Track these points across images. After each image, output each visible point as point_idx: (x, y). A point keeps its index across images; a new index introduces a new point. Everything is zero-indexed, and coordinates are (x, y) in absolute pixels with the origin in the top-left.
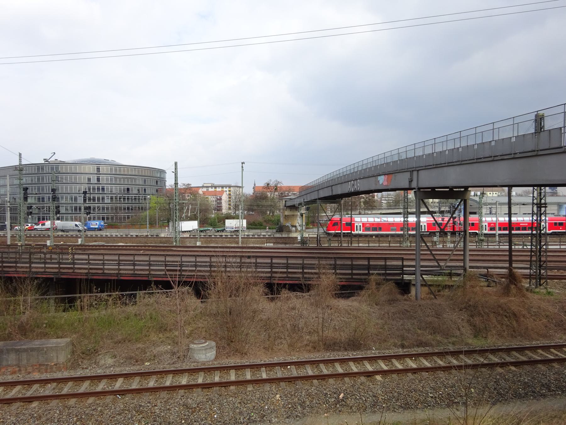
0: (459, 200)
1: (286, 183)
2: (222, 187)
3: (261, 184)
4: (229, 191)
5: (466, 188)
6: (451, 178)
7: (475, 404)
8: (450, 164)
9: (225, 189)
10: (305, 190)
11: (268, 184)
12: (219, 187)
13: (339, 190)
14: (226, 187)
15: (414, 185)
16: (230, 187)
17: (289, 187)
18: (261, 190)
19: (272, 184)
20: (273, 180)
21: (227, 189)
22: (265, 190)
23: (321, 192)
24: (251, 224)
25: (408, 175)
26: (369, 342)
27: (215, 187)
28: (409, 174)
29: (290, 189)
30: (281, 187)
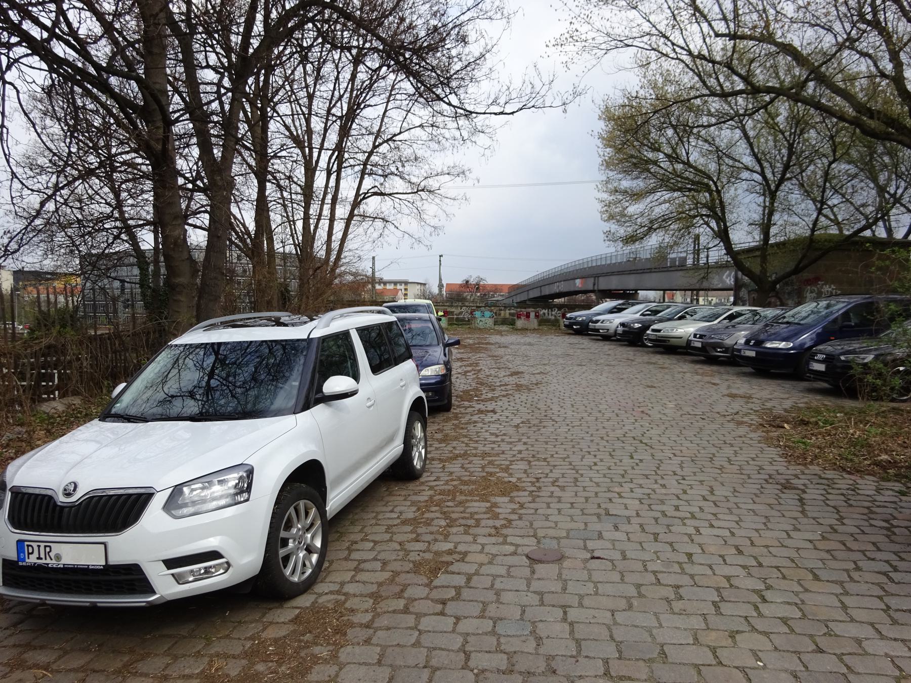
0: (186, 227)
1: (492, 279)
2: (395, 283)
3: (459, 280)
4: (406, 289)
5: (636, 290)
6: (629, 282)
7: (48, 431)
8: (612, 274)
9: (399, 287)
10: (516, 289)
11: (467, 282)
12: (390, 282)
13: (547, 291)
14: (401, 283)
15: (596, 288)
16: (406, 283)
17: (495, 285)
18: (457, 289)
19: (473, 281)
20: (474, 276)
21: (403, 287)
22: (463, 289)
23: (531, 292)
24: (284, 304)
25: (592, 279)
26: (427, 112)
27: (385, 283)
28: (592, 279)
29: (496, 289)
30: (484, 286)
